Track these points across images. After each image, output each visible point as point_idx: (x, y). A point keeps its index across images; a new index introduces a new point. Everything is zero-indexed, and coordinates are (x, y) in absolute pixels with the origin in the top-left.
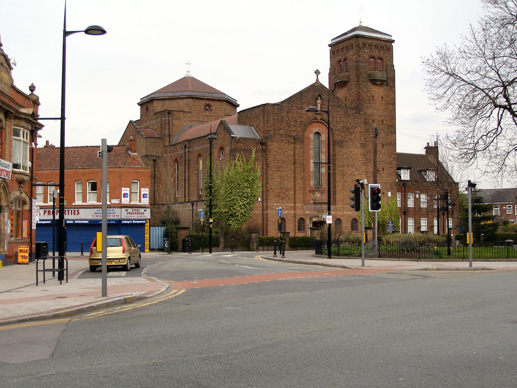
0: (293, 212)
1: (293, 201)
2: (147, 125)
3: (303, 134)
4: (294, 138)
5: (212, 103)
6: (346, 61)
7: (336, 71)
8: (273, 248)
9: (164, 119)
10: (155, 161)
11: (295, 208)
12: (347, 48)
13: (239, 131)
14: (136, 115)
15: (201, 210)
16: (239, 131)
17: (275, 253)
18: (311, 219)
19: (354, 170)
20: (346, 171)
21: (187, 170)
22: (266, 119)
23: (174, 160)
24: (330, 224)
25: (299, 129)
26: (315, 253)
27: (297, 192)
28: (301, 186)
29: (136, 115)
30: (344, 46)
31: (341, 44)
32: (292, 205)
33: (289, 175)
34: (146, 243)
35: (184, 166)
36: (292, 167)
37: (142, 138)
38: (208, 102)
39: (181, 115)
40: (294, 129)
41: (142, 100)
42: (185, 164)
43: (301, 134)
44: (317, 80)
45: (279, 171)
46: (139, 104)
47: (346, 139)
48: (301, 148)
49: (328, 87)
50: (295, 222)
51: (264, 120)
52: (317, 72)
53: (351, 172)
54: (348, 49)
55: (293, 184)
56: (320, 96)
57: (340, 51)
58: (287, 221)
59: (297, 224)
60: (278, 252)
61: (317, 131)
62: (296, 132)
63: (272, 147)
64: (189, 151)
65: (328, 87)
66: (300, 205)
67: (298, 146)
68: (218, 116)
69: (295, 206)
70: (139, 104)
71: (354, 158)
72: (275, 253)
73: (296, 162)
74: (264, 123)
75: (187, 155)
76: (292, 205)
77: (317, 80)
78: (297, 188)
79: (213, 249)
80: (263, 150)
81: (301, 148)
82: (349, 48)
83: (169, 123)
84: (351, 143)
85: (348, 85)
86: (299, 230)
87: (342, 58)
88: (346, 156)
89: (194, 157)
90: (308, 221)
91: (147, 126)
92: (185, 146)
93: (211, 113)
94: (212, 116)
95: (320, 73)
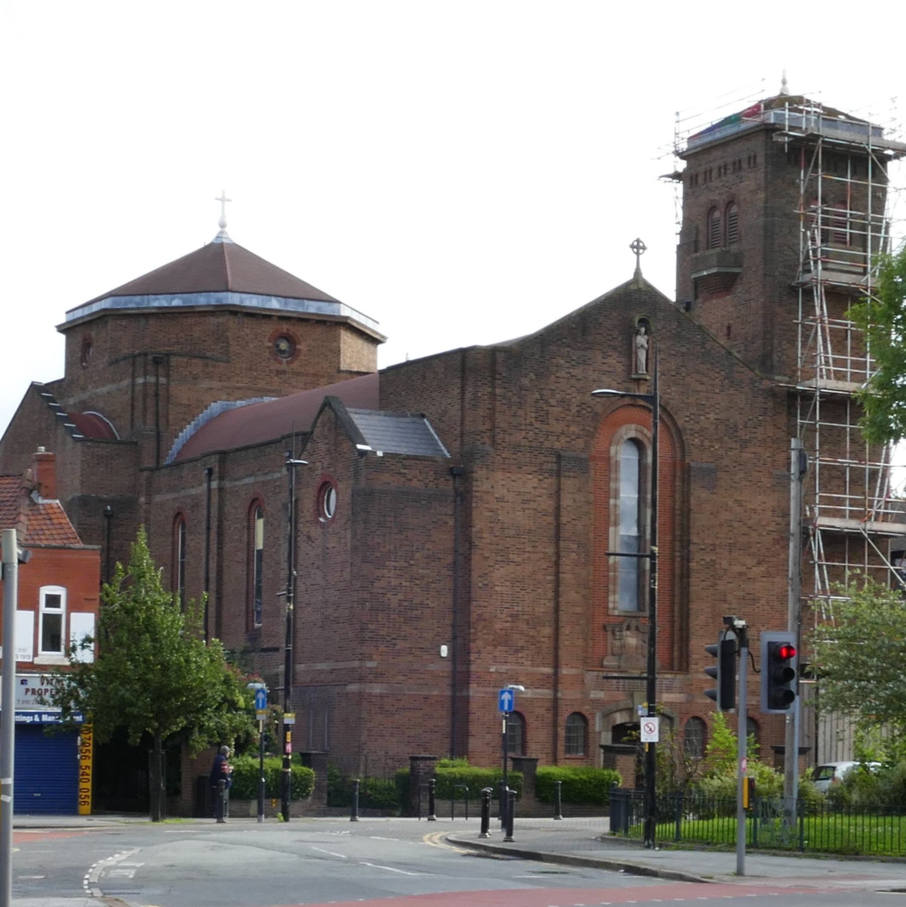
0: (547, 693)
1: (550, 659)
2: (84, 396)
3: (587, 446)
4: (559, 457)
5: (298, 330)
6: (734, 209)
7: (702, 238)
8: (475, 806)
9: (140, 381)
10: (108, 516)
11: (555, 681)
12: (737, 166)
13: (376, 435)
14: (51, 365)
15: (258, 686)
16: (377, 435)
17: (485, 827)
18: (607, 715)
19: (750, 561)
20: (725, 564)
21: (214, 548)
22: (468, 396)
23: (172, 513)
24: (651, 745)
25: (573, 428)
26: (607, 829)
27: (565, 631)
28: (578, 610)
29: (51, 365)
30: (730, 160)
31: (717, 153)
32: (548, 670)
33: (540, 577)
34: (82, 785)
35: (204, 537)
36: (551, 550)
37: (69, 440)
38: (285, 327)
39: (197, 366)
40: (558, 427)
41: (72, 317)
42: (208, 528)
43: (580, 443)
44: (638, 273)
45: (509, 562)
46: (62, 329)
47: (725, 462)
48: (579, 490)
49: (672, 296)
50: (555, 724)
51: (462, 399)
52: (638, 247)
53: (738, 568)
54: (740, 168)
55: (551, 605)
56: (643, 322)
57: (715, 173)
58: (530, 720)
59: (562, 732)
60: (494, 821)
61: (632, 434)
62: (563, 439)
63: (486, 486)
64: (221, 489)
65: (672, 296)
66: (574, 671)
67: (569, 484)
68: (315, 375)
69: (556, 674)
70: (62, 329)
71: (750, 523)
72: (485, 827)
73: (564, 534)
74: (462, 408)
75: (215, 500)
76: (548, 670)
77: (638, 273)
78: (563, 617)
79: (293, 807)
80: (457, 493)
81: (579, 490)
82: (745, 165)
83: (157, 395)
84: (741, 475)
85: (739, 288)
86: (568, 750)
87: (718, 197)
88: (725, 516)
89: (236, 509)
90: (597, 724)
91: (83, 402)
92: (210, 471)
93: (295, 365)
94: (298, 374)
95: (644, 248)
